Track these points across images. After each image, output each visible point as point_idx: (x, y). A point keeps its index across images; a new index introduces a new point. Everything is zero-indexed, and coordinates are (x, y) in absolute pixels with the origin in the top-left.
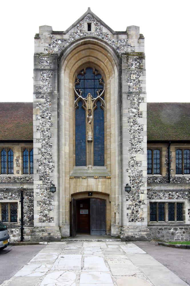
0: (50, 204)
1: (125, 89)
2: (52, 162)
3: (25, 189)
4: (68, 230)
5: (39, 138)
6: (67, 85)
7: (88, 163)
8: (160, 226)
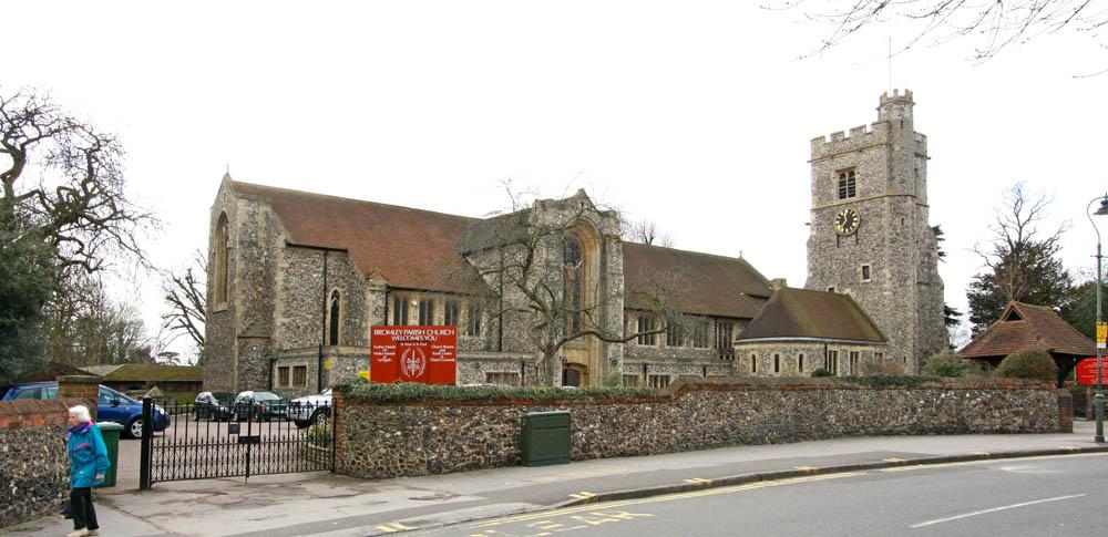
1: (609, 270)
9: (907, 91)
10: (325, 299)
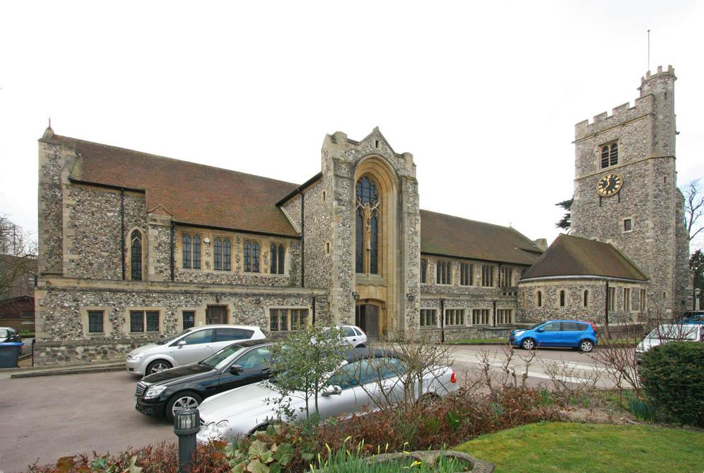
0: (349, 311)
1: (405, 209)
9: (670, 67)
10: (123, 237)
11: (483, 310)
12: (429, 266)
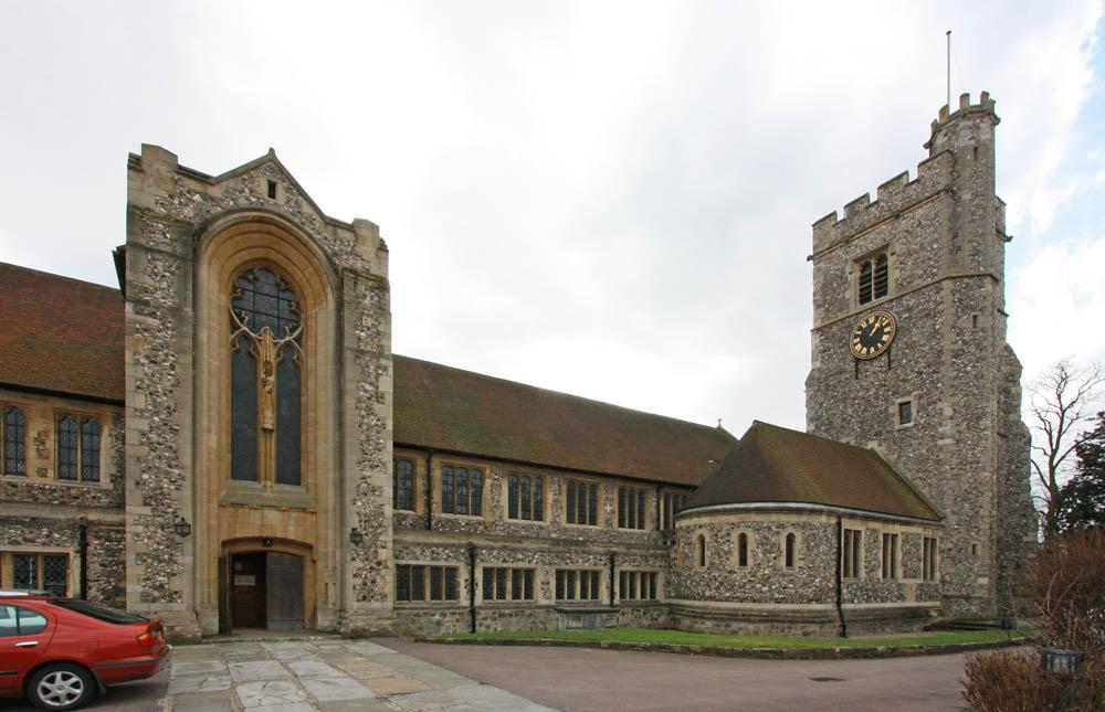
0: (172, 561)
1: (349, 342)
2: (177, 467)
3: (92, 523)
4: (216, 621)
5: (143, 407)
6: (214, 297)
7: (263, 476)
8: (416, 609)
9: (985, 95)
11: (584, 573)
12: (488, 482)
